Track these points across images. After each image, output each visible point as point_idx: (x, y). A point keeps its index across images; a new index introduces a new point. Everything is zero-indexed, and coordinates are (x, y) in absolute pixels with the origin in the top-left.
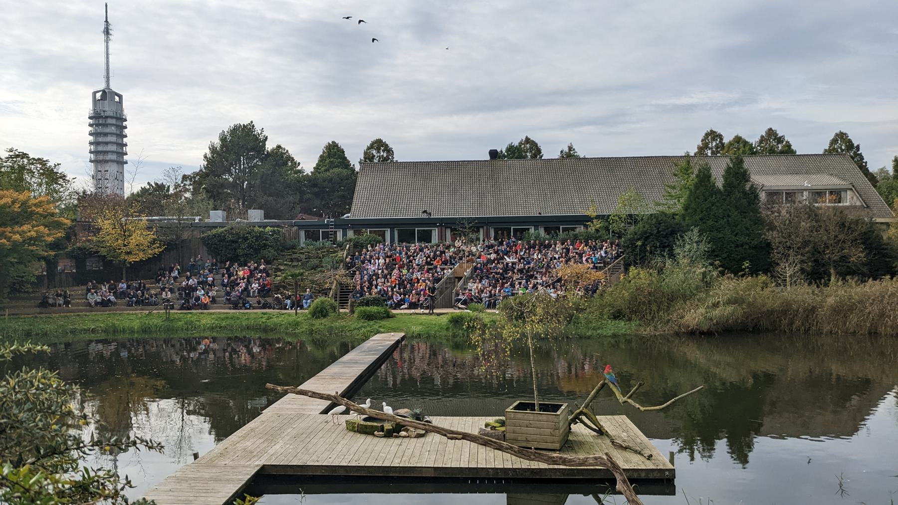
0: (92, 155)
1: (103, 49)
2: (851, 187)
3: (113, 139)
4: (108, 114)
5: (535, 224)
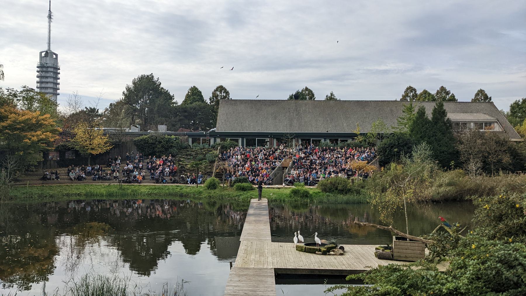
0: (38, 89)
1: (47, 27)
2: (497, 121)
3: (51, 80)
4: (49, 65)
5: (215, 136)
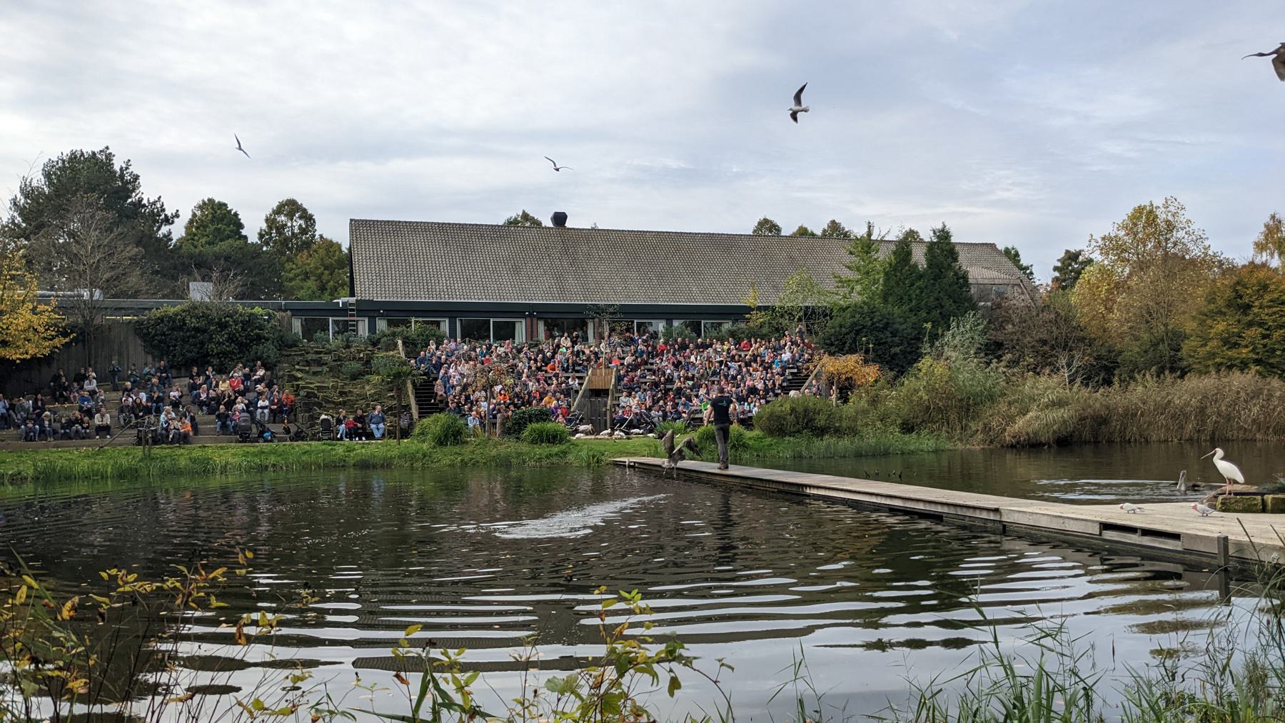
5: (372, 314)
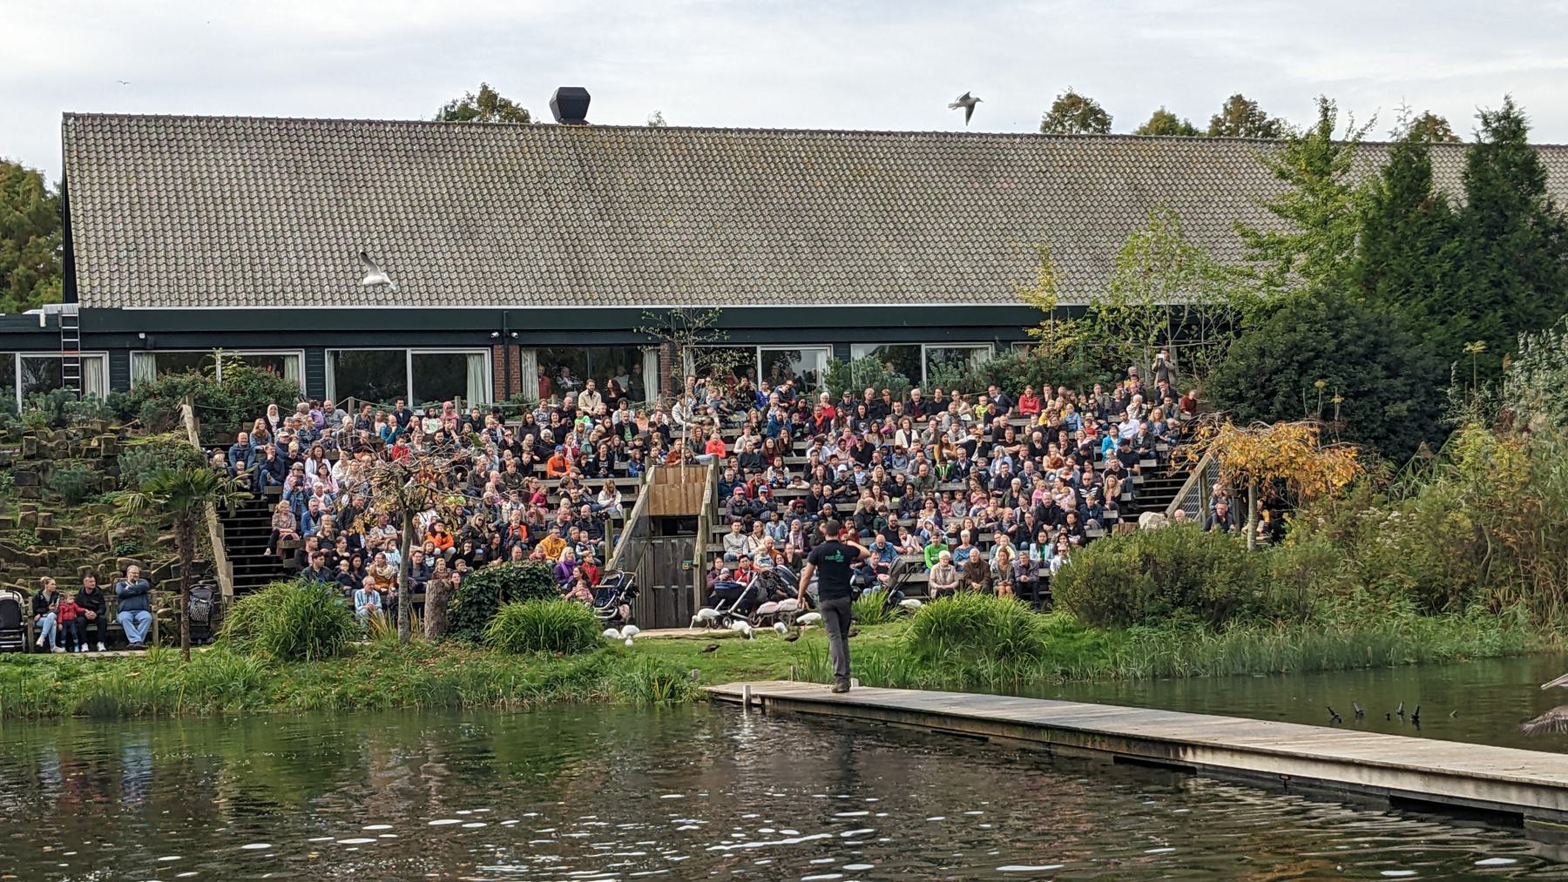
5: (116, 343)
